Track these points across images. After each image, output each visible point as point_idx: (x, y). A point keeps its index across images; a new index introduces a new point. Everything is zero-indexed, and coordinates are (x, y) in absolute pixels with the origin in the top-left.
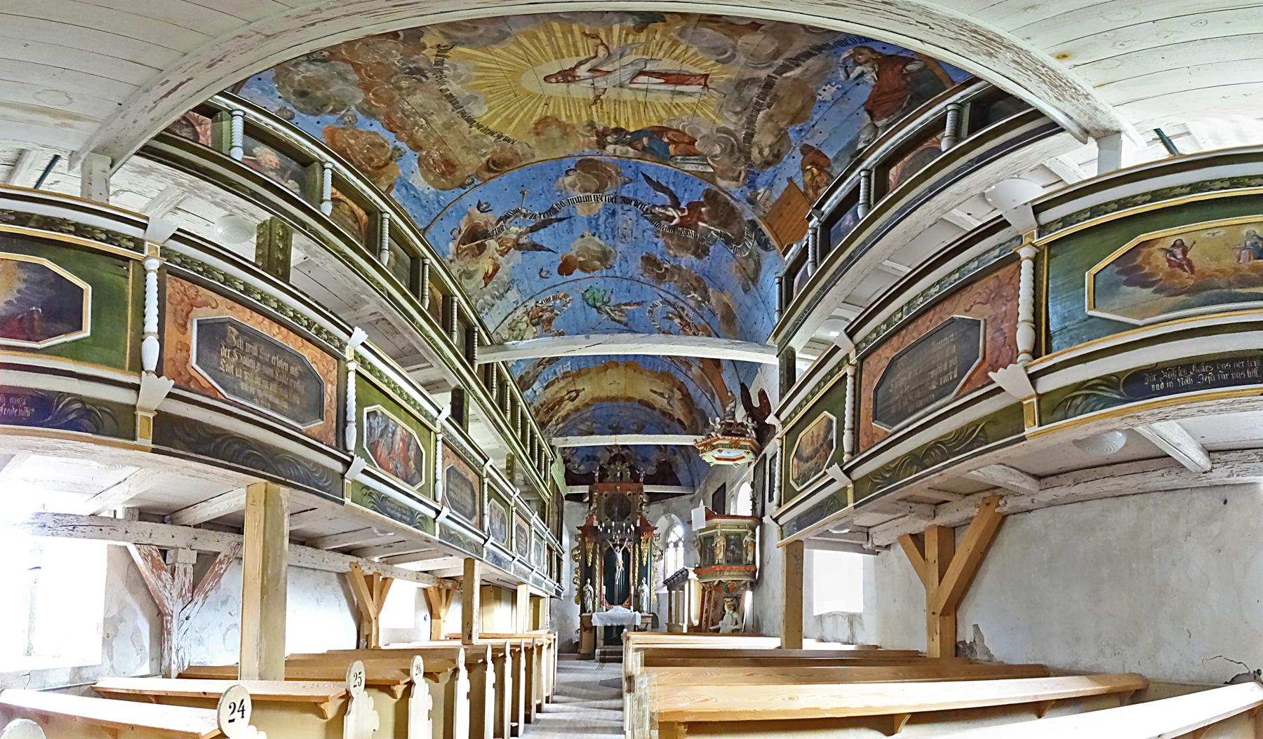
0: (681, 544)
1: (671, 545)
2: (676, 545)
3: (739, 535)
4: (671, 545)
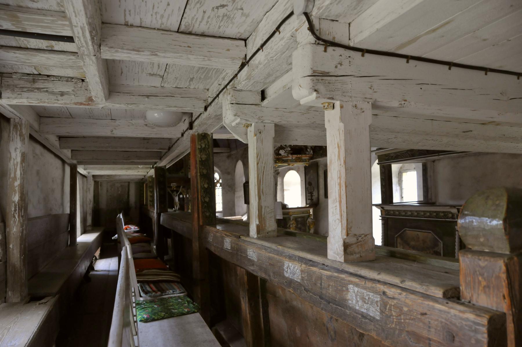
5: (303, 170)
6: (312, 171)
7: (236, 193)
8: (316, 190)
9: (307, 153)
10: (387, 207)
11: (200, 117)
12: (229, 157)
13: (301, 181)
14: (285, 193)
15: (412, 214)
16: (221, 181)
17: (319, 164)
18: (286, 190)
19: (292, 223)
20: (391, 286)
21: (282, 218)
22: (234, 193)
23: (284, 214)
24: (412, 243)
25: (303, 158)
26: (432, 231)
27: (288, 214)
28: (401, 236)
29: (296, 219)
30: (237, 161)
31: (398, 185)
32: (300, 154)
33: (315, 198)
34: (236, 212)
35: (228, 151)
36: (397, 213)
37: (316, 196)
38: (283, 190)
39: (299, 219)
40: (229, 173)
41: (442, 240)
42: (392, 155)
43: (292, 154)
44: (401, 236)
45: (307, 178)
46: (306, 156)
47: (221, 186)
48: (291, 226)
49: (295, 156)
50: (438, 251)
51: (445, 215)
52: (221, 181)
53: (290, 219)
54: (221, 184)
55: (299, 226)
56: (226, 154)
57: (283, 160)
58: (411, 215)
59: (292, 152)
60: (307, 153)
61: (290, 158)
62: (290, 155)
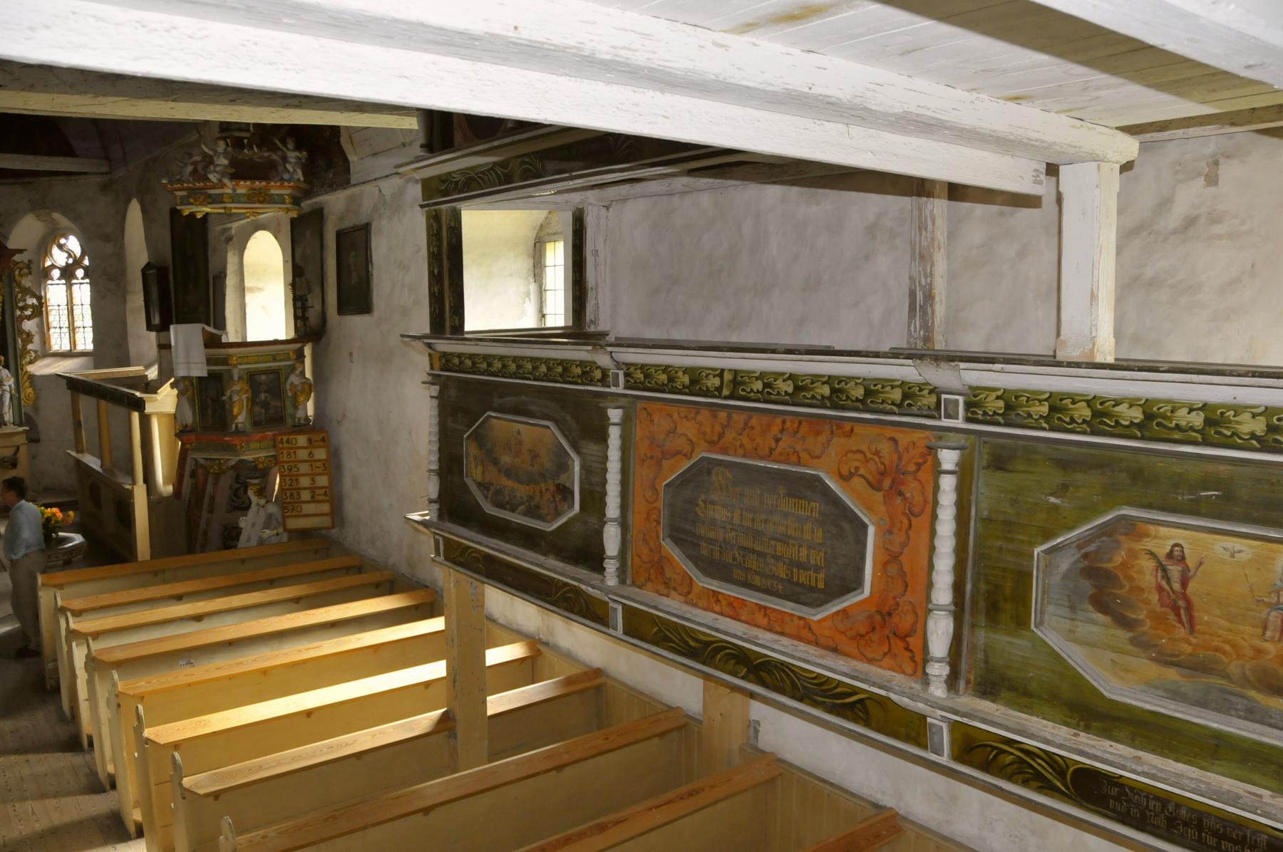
0: (80, 273)
1: (56, 273)
2: (67, 273)
3: (275, 372)
4: (56, 273)
5: (287, 228)
6: (308, 233)
7: (129, 297)
8: (317, 290)
9: (286, 176)
10: (444, 346)
11: (644, 184)
12: (105, 188)
13: (285, 262)
14: (249, 298)
15: (504, 366)
16: (86, 262)
17: (326, 212)
18: (252, 290)
19: (237, 388)
20: (253, 613)
21: (205, 374)
22: (125, 301)
23: (210, 361)
24: (506, 459)
25: (273, 192)
26: (557, 422)
27: (225, 361)
28: (478, 437)
29: (251, 377)
30: (128, 202)
31: (532, 280)
32: (260, 179)
33: (313, 315)
34: (132, 352)
35: (105, 169)
36: (468, 363)
37: (318, 307)
38: (242, 290)
39: (263, 377)
40: (107, 238)
41: (578, 453)
42: (458, 177)
43: (234, 177)
44: (478, 437)
45: (299, 251)
46: (282, 187)
47: (86, 276)
48: (236, 398)
49: (243, 187)
50: (568, 485)
51: (584, 373)
52: (86, 262)
53: (231, 377)
54: (86, 269)
55: (263, 396)
56: (98, 179)
57: (210, 196)
58: (502, 372)
59: (233, 171)
60: (286, 176)
61: (230, 191)
62: (226, 181)
